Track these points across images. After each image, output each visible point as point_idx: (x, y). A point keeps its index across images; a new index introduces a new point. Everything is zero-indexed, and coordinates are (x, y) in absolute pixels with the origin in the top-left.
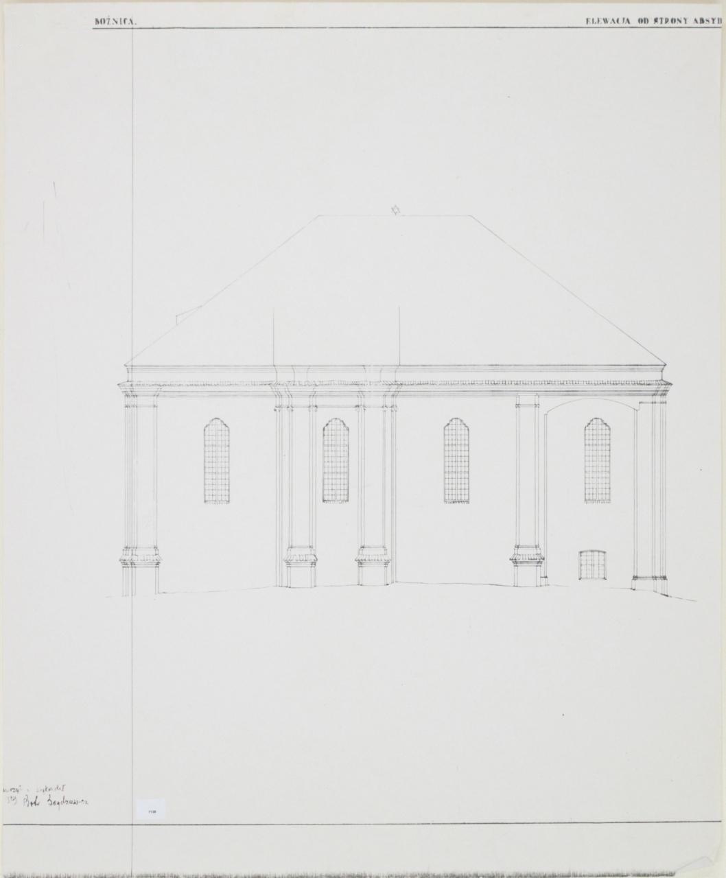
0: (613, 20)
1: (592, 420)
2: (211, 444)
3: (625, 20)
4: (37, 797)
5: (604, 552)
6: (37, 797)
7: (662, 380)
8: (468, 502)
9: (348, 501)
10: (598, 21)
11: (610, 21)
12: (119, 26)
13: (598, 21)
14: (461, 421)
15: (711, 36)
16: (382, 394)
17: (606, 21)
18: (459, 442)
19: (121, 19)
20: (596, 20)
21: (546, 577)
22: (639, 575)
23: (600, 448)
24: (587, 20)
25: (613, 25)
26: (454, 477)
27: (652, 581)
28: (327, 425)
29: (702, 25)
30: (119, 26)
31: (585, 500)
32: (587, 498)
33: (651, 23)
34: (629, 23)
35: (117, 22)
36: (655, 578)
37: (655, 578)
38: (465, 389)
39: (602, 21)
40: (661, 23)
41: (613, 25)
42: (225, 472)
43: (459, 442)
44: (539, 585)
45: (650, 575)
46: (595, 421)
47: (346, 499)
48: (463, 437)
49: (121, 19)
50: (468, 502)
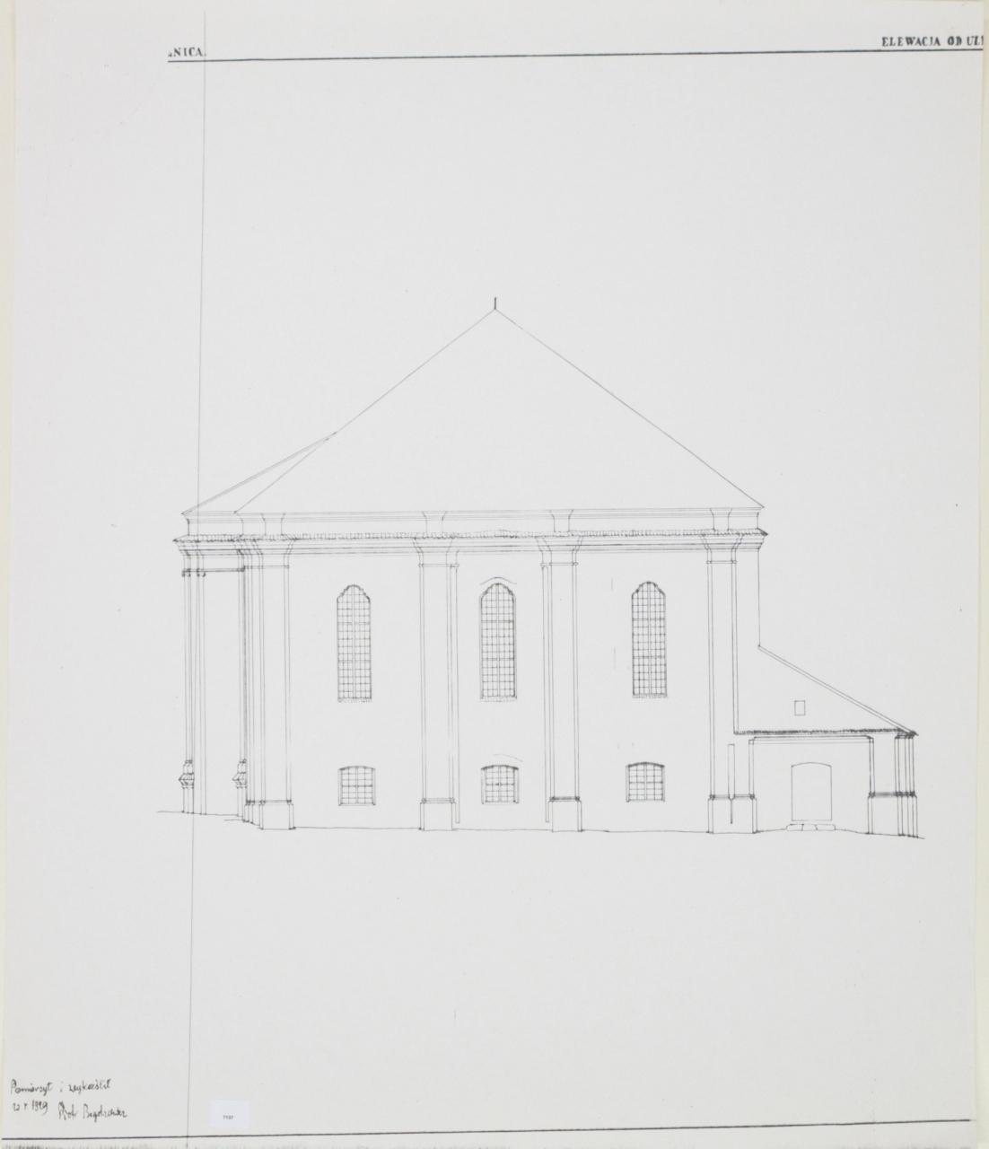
0: (919, 40)
1: (641, 585)
2: (489, 619)
3: (934, 40)
4: (73, 1106)
5: (662, 766)
6: (73, 1106)
7: (714, 529)
8: (665, 695)
9: (371, 698)
10: (900, 42)
11: (182, 52)
12: (182, 57)
13: (900, 42)
14: (655, 585)
15: (968, 61)
16: (572, 548)
17: (909, 41)
18: (653, 616)
19: (185, 49)
20: (895, 41)
21: (577, 799)
22: (557, 796)
23: (653, 623)
24: (884, 39)
25: (918, 47)
26: (350, 667)
27: (895, 799)
28: (637, 591)
29: (910, 47)
30: (182, 57)
31: (339, 698)
32: (342, 696)
33: (944, 45)
34: (939, 44)
35: (179, 54)
36: (899, 794)
37: (899, 794)
38: (508, 541)
39: (904, 41)
40: (185, 54)
41: (918, 47)
42: (661, 657)
43: (653, 616)
44: (203, 812)
45: (892, 789)
46: (645, 587)
47: (512, 694)
48: (506, 610)
49: (185, 49)
50: (665, 695)
